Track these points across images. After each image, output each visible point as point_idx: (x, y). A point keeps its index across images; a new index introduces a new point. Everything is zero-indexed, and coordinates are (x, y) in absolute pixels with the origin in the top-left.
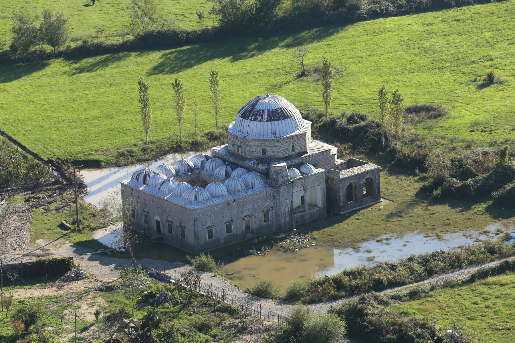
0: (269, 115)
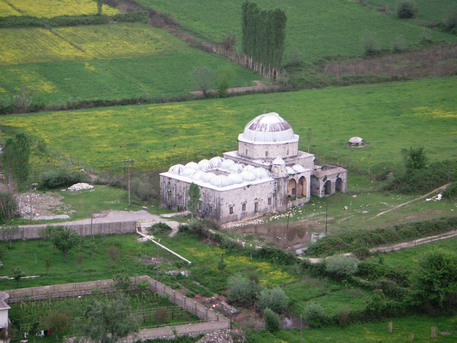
0: (271, 128)
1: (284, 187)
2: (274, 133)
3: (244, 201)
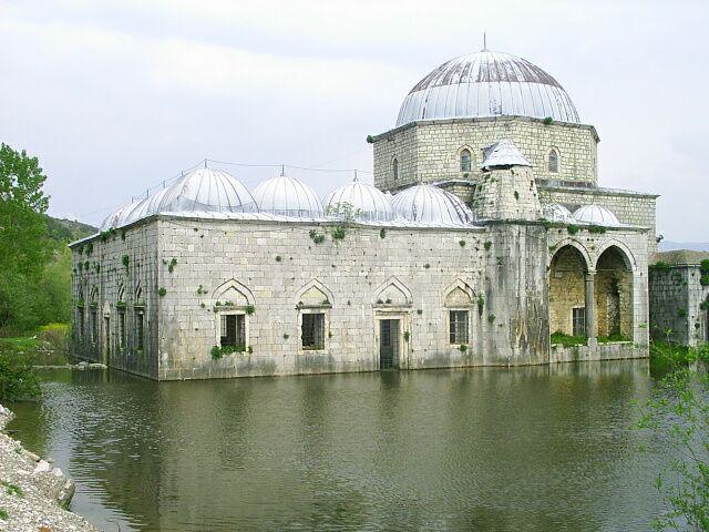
1: (531, 267)
2: (495, 85)
3: (314, 298)
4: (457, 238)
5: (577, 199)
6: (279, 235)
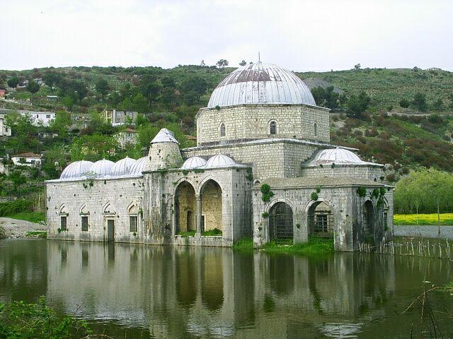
1: (154, 195)
4: (132, 182)
5: (208, 152)
6: (75, 186)
